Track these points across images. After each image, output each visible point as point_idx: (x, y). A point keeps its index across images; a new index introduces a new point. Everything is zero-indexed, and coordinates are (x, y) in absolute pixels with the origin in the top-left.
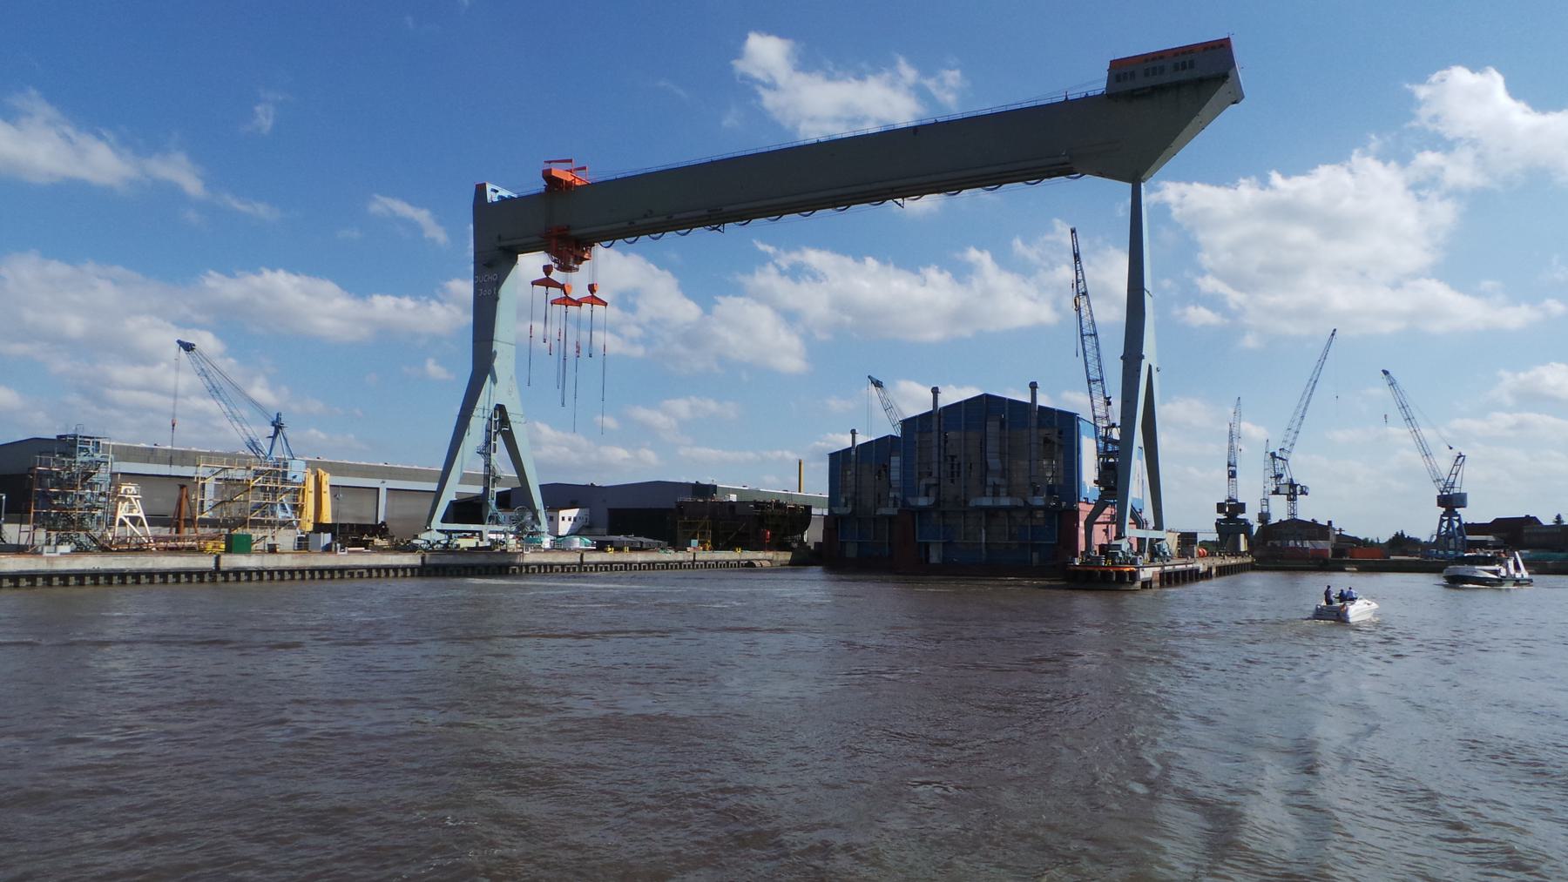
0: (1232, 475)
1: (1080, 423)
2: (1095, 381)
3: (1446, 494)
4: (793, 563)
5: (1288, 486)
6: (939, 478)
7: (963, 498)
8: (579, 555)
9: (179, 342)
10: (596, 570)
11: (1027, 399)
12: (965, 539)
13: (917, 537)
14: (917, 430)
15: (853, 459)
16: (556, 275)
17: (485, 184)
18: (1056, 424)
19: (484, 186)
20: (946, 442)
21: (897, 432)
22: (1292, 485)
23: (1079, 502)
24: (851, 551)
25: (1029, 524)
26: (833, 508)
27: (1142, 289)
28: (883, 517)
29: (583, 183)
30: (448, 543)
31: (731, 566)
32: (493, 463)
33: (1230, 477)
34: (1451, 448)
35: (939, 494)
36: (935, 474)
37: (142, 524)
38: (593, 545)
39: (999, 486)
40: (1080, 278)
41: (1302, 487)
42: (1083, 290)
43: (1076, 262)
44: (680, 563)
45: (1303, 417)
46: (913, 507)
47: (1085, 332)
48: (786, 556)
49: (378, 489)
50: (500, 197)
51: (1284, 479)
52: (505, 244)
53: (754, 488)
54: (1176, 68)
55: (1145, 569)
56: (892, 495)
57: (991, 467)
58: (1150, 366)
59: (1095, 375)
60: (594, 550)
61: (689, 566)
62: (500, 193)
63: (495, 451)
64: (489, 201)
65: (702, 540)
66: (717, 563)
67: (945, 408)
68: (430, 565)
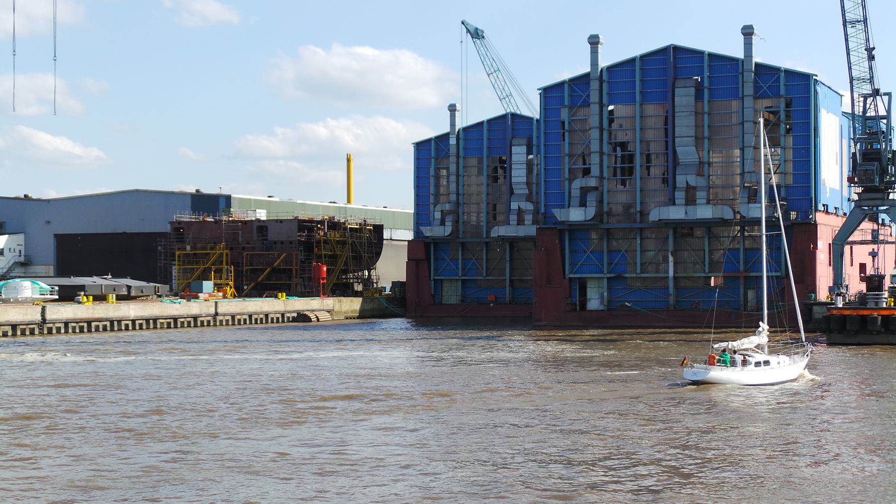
1: (818, 88)
2: (854, 23)
4: (363, 315)
7: (638, 209)
8: (39, 309)
10: (66, 332)
11: (739, 54)
12: (642, 272)
13: (567, 272)
14: (566, 103)
15: (453, 150)
21: (531, 108)
23: (816, 210)
24: (451, 295)
26: (423, 229)
28: (503, 239)
31: (272, 322)
35: (600, 202)
36: (595, 171)
39: (694, 188)
46: (563, 223)
48: (354, 304)
53: (285, 198)
56: (514, 206)
61: (209, 322)
65: (219, 282)
66: (233, 317)
67: (610, 68)
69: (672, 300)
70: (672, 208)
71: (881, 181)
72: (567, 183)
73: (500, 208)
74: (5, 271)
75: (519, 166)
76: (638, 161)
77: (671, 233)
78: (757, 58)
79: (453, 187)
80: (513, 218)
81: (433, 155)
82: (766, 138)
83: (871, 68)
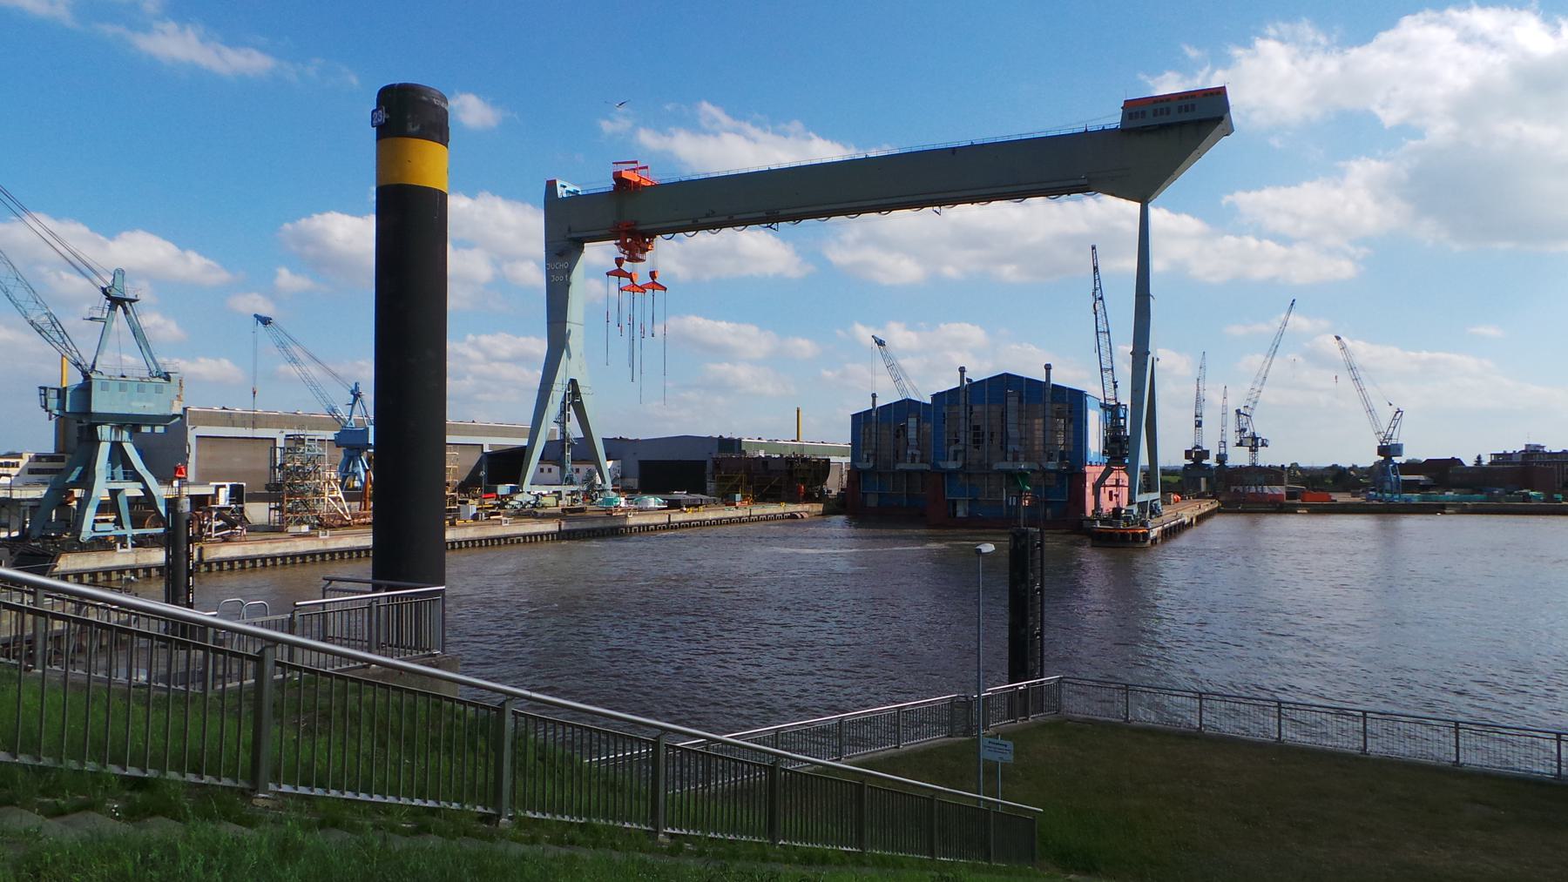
0: (1199, 424)
2: (1107, 370)
3: (1384, 444)
4: (825, 513)
5: (1250, 440)
6: (966, 445)
7: (986, 461)
9: (256, 316)
12: (989, 497)
13: (946, 493)
15: (874, 420)
16: (626, 266)
17: (555, 181)
18: (1067, 400)
20: (971, 414)
22: (1254, 438)
29: (649, 184)
30: (535, 503)
32: (568, 430)
33: (1196, 426)
34: (1391, 405)
35: (965, 458)
37: (341, 500)
38: (664, 504)
40: (1097, 286)
41: (1263, 440)
44: (740, 518)
46: (944, 469)
48: (819, 508)
50: (568, 192)
51: (1248, 433)
52: (574, 235)
54: (1180, 109)
57: (1011, 436)
60: (1369, 712)
62: (567, 189)
63: (569, 421)
64: (559, 195)
68: (565, 531)
69: (1005, 512)
70: (1005, 463)
71: (1121, 453)
72: (946, 448)
73: (901, 452)
76: (987, 435)
77: (1005, 476)
78: (1053, 381)
80: (909, 459)
83: (1115, 394)
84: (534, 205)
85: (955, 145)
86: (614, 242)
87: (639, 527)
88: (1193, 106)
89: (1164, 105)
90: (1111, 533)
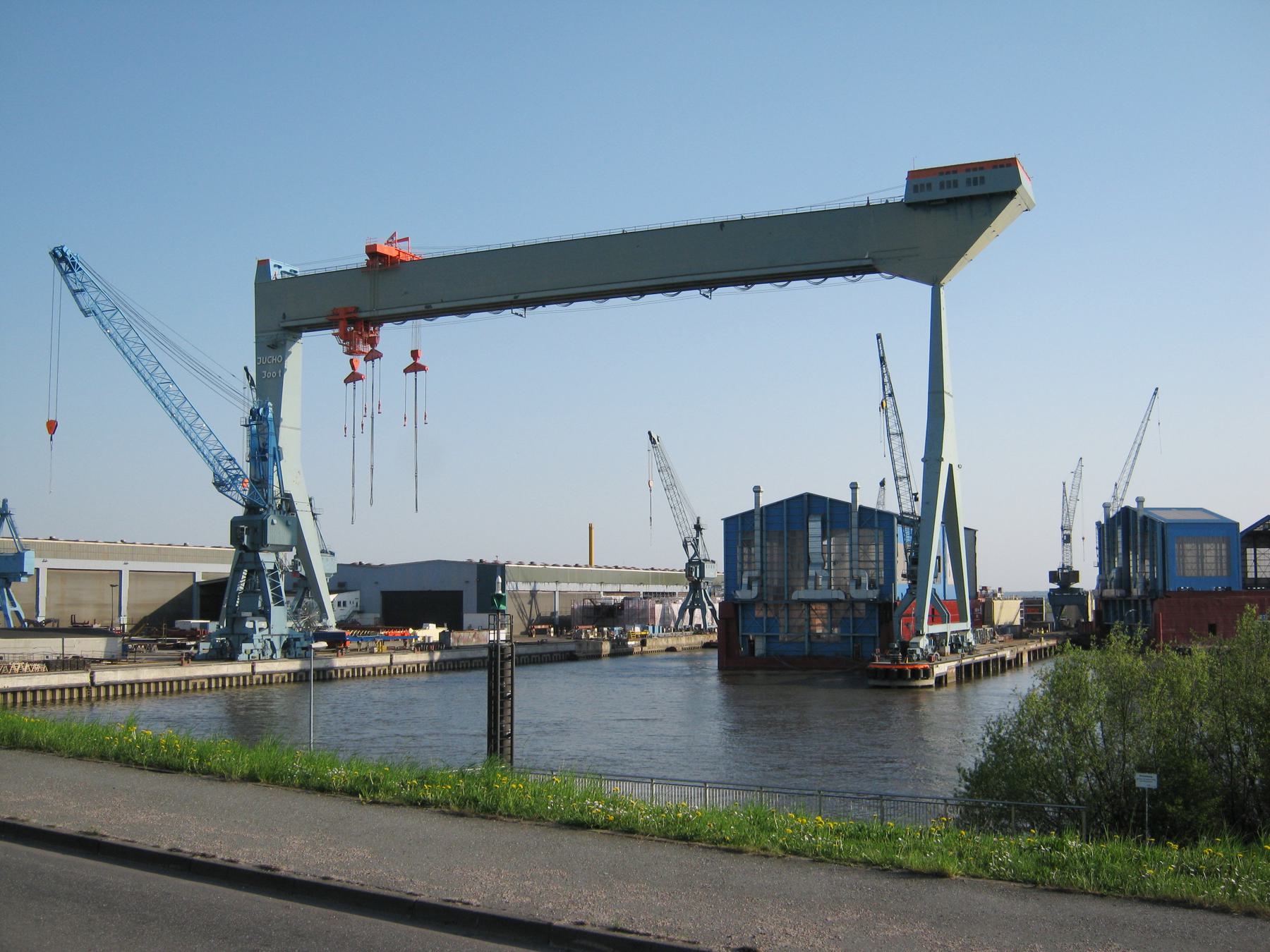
0: (1067, 540)
11: (849, 500)
13: (740, 630)
19: (267, 262)
25: (851, 617)
27: (942, 392)
29: (409, 258)
40: (886, 380)
42: (889, 392)
43: (882, 366)
45: (1127, 483)
47: (891, 431)
49: (121, 571)
55: (939, 665)
56: (812, 573)
58: (951, 466)
59: (901, 473)
62: (282, 269)
64: (273, 278)
74: (346, 617)
75: (815, 539)
79: (758, 557)
81: (739, 529)
82: (946, 538)
84: (1023, 188)
85: (724, 219)
86: (331, 331)
87: (353, 670)
88: (982, 179)
89: (952, 177)
90: (887, 669)
